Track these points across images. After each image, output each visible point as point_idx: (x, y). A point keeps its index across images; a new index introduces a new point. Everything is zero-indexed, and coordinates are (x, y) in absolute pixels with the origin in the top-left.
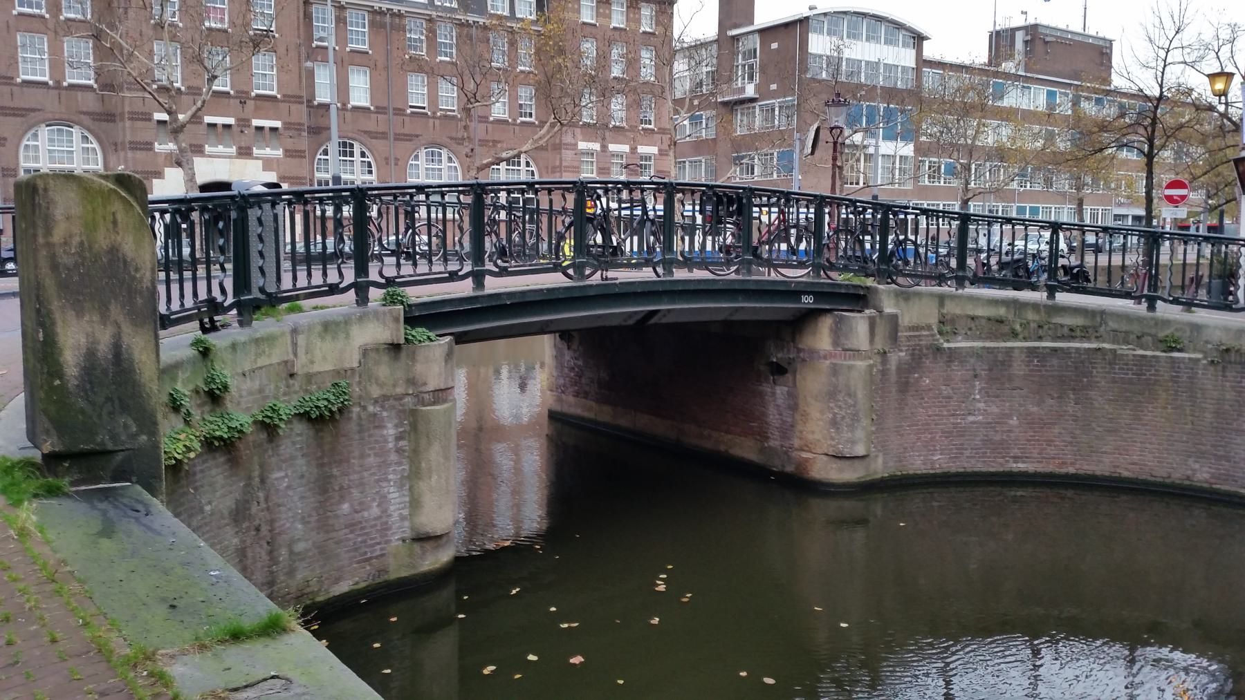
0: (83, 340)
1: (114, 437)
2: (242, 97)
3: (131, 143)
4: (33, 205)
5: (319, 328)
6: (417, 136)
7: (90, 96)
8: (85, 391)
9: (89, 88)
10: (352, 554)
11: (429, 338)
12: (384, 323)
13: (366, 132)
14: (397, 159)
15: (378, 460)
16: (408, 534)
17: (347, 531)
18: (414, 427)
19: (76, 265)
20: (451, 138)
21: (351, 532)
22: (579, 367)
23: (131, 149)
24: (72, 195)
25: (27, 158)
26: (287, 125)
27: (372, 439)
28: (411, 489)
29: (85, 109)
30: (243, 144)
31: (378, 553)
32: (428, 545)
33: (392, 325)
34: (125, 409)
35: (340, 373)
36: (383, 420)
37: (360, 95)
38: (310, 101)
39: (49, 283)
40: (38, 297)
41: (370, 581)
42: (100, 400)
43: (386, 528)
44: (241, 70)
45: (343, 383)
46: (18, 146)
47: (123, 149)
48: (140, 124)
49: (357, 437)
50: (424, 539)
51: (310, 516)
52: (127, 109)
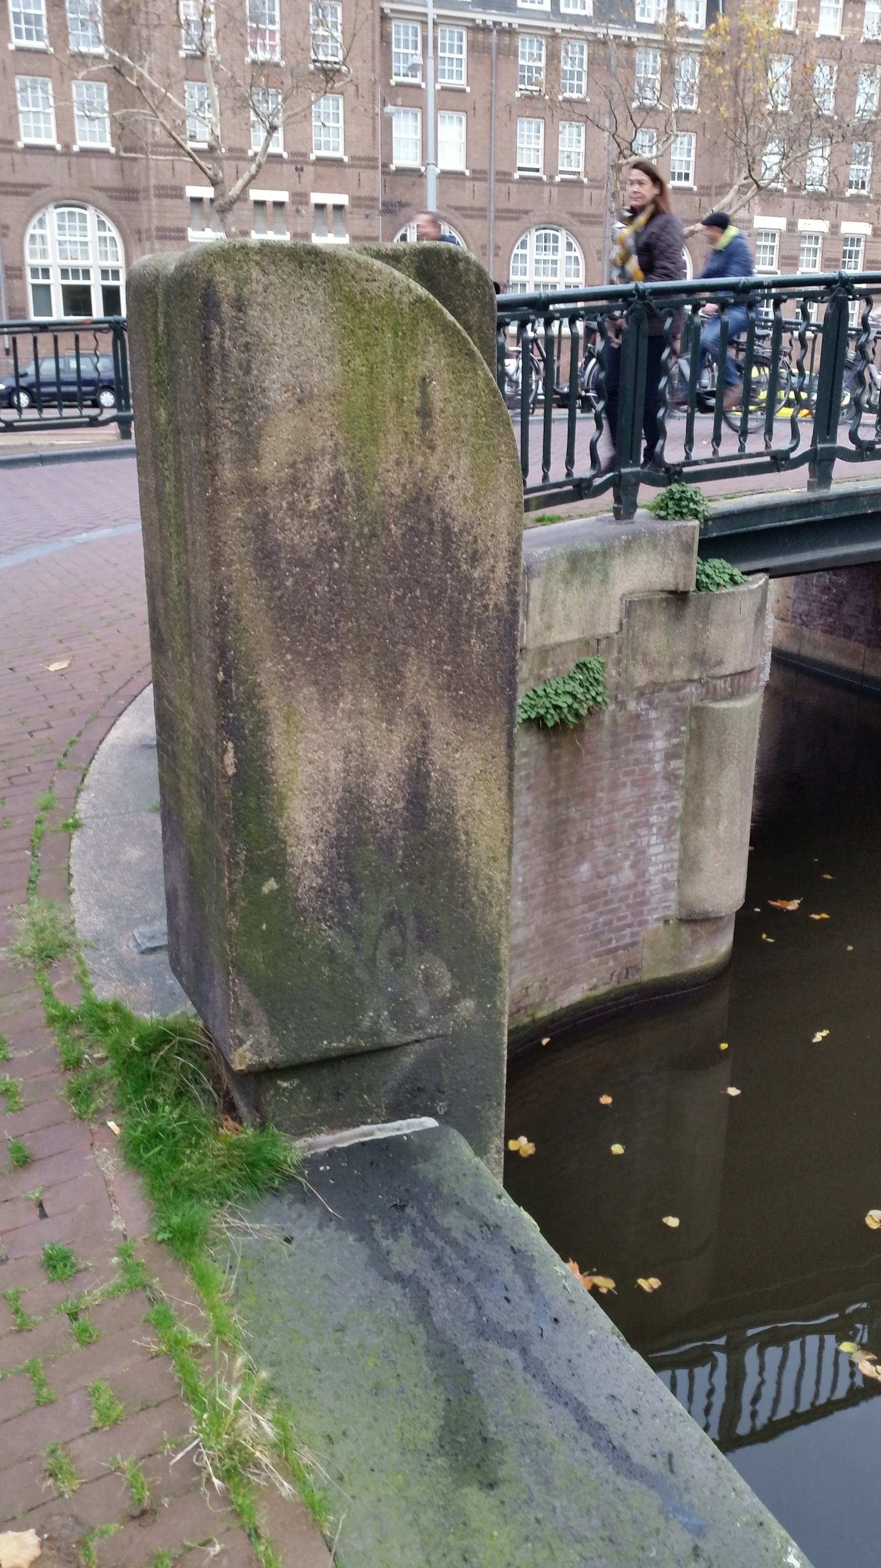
0: (336, 766)
1: (401, 1011)
2: (299, 161)
3: (158, 229)
4: (206, 354)
5: (563, 565)
6: (526, 212)
7: (107, 165)
8: (338, 903)
9: (104, 153)
10: (590, 943)
11: (732, 577)
12: (665, 555)
13: (457, 208)
14: (497, 248)
15: (637, 792)
16: (673, 912)
17: (584, 907)
18: (698, 737)
19: (323, 551)
20: (574, 215)
21: (591, 909)
22: (838, 586)
23: (160, 238)
24: (314, 321)
25: (33, 254)
26: (356, 201)
27: (631, 758)
28: (683, 839)
29: (101, 184)
30: (299, 230)
31: (627, 940)
32: (701, 930)
33: (677, 557)
34: (428, 938)
35: (593, 644)
36: (649, 726)
37: (452, 155)
38: (385, 165)
39: (251, 606)
40: (222, 649)
41: (614, 984)
42: (372, 920)
43: (641, 901)
44: (299, 119)
45: (594, 664)
46: (22, 237)
47: (149, 238)
48: (169, 202)
49: (608, 754)
50: (695, 920)
51: (535, 886)
52: (153, 182)
